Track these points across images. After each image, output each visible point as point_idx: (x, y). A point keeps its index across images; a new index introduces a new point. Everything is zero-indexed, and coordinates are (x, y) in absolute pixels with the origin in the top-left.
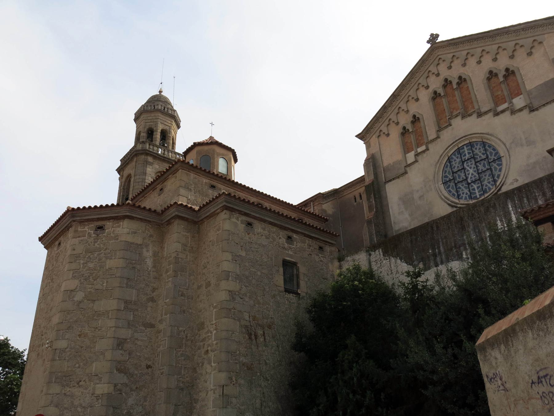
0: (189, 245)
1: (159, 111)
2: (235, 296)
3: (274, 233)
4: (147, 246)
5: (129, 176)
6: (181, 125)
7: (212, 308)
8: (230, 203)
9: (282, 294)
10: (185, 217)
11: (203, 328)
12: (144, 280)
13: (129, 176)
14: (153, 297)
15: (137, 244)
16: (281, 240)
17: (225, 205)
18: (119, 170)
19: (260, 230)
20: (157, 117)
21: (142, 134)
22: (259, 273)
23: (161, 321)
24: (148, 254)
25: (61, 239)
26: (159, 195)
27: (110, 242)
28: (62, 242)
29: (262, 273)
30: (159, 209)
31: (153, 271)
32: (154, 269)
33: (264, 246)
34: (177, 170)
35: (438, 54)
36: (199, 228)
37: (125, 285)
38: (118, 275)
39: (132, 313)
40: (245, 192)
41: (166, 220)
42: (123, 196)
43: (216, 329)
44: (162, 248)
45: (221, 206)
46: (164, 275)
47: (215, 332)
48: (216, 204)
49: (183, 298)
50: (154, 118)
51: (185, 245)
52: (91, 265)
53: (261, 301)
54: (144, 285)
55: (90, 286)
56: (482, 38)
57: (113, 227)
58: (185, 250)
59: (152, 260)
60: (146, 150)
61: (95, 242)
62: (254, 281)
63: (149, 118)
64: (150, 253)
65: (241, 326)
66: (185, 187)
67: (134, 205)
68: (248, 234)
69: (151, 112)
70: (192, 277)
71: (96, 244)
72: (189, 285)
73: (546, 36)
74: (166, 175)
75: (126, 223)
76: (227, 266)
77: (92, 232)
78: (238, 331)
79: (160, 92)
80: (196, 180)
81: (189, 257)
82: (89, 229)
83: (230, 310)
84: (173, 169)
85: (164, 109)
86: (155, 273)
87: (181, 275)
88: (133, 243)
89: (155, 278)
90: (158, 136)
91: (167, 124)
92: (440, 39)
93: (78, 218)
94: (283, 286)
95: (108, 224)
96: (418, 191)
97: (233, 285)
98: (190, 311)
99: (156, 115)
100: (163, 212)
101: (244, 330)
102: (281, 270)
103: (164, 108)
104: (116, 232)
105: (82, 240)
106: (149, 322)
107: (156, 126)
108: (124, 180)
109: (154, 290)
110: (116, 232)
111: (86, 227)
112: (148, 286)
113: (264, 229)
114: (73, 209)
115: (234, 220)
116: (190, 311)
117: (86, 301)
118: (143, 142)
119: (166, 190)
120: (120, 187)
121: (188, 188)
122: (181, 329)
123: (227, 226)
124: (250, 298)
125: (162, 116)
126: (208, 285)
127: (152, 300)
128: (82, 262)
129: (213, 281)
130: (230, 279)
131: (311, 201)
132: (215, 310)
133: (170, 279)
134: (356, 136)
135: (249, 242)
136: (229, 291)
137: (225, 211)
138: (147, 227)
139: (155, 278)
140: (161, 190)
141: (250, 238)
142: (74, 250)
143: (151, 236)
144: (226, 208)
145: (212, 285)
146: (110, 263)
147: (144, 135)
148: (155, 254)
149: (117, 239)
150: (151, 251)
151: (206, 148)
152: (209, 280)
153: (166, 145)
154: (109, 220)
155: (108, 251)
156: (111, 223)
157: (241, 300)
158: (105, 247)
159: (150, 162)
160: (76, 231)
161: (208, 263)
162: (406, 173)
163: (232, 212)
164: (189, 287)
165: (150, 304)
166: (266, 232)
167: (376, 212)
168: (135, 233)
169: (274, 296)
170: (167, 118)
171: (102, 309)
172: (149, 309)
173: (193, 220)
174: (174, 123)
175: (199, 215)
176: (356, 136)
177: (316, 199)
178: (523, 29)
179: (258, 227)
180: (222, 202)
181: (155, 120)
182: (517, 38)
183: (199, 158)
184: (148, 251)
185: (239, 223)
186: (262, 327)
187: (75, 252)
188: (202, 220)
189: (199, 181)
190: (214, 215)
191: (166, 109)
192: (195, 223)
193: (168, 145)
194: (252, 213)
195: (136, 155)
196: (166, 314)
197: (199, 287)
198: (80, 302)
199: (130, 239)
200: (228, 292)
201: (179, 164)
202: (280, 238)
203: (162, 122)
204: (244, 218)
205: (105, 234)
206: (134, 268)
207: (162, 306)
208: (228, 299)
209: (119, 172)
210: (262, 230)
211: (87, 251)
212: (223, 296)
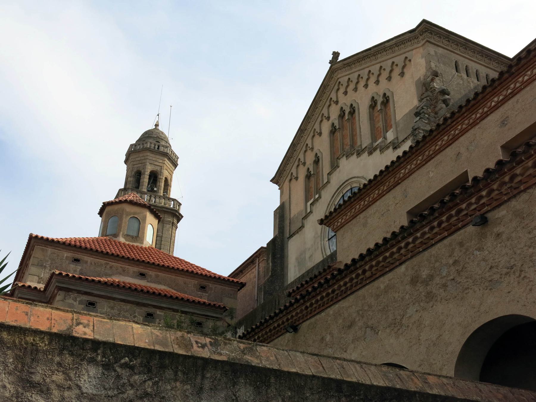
1: (149, 150)
3: (127, 311)
6: (178, 163)
20: (146, 157)
35: (339, 76)
40: (121, 262)
50: (143, 158)
56: (391, 47)
63: (137, 159)
66: (38, 265)
69: (139, 151)
73: (414, 51)
79: (157, 125)
80: (55, 255)
90: (145, 180)
91: (158, 164)
92: (340, 58)
96: (309, 249)
99: (145, 154)
107: (144, 168)
113: (112, 308)
115: (71, 301)
121: (42, 266)
131: (256, 257)
134: (271, 181)
144: (60, 289)
151: (116, 207)
153: (155, 189)
162: (303, 227)
167: (272, 276)
170: (157, 157)
174: (167, 162)
176: (271, 181)
177: (260, 254)
178: (397, 45)
181: (143, 161)
182: (394, 55)
189: (58, 256)
193: (158, 189)
194: (94, 292)
203: (152, 162)
204: (85, 298)
210: (109, 309)
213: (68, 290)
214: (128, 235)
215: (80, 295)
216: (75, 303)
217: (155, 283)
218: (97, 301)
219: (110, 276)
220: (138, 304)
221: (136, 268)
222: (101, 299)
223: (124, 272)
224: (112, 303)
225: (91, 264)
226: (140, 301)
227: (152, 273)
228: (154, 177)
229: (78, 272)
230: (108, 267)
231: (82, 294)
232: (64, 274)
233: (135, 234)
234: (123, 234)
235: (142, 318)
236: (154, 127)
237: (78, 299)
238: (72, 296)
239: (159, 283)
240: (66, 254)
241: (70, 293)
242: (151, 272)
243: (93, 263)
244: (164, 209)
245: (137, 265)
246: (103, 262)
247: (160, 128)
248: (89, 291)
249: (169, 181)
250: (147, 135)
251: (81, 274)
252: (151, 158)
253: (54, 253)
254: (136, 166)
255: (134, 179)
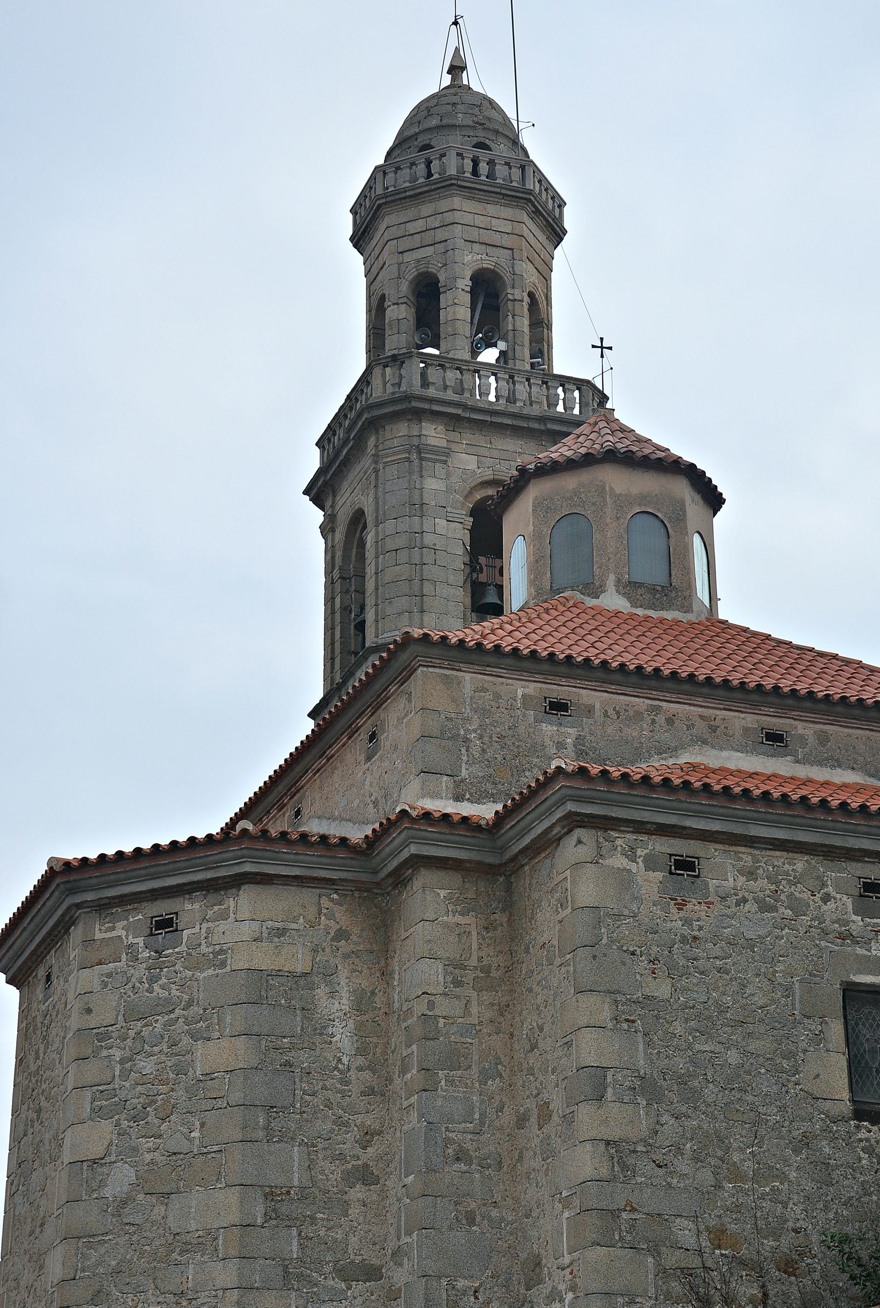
0: (474, 962)
2: (631, 1161)
4: (329, 975)
5: (358, 519)
7: (558, 1206)
8: (589, 801)
9: (842, 1128)
10: (447, 859)
11: (540, 1281)
12: (329, 1105)
13: (358, 519)
14: (366, 1165)
15: (292, 974)
16: (831, 905)
17: (570, 814)
18: (319, 491)
19: (732, 881)
20: (449, 217)
21: (392, 313)
22: (733, 1057)
23: (397, 1254)
24: (336, 1005)
25: (52, 959)
26: (369, 759)
27: (201, 976)
28: (55, 970)
29: (745, 1053)
30: (357, 834)
31: (360, 1069)
32: (360, 1061)
33: (750, 944)
34: (408, 672)
36: (509, 888)
37: (261, 1134)
38: (236, 1097)
39: (294, 1232)
40: (700, 701)
41: (385, 871)
42: (346, 609)
43: (573, 1288)
44: (385, 974)
45: (559, 814)
46: (397, 1081)
47: (570, 1296)
48: (543, 808)
49: (463, 1167)
50: (435, 222)
51: (455, 965)
52: (147, 1066)
53: (748, 1166)
54: (329, 1126)
55: (151, 1143)
57: (204, 919)
58: (458, 983)
59: (351, 1024)
60: (408, 398)
61: (153, 980)
62: (710, 1092)
63: (412, 227)
64: (344, 1002)
65: (663, 1272)
67: (265, 832)
68: (680, 906)
70: (493, 1085)
71: (156, 987)
72: (483, 1115)
74: (377, 686)
75: (245, 902)
76: (591, 1049)
77: (140, 941)
78: (652, 1291)
79: (457, 69)
80: (488, 696)
81: (474, 1010)
82: (126, 930)
83: (614, 1214)
84: (397, 665)
85: (475, 172)
86: (367, 1075)
87: (450, 1082)
88: (279, 973)
89: (370, 1092)
90: (457, 308)
91: (496, 239)
93: (90, 896)
94: (846, 1095)
95: (190, 909)
97: (621, 1119)
98: (495, 1213)
99: (443, 205)
100: (372, 842)
101: (676, 1286)
102: (836, 1030)
103: (475, 162)
104: (216, 939)
105: (109, 975)
106: (358, 1259)
108: (339, 535)
109: (368, 1137)
110: (216, 939)
111: (120, 925)
112: (346, 1124)
113: (751, 875)
114: (67, 864)
115: (619, 861)
116: (495, 1213)
117: (141, 1197)
118: (394, 358)
119: (386, 739)
120: (328, 572)
122: (461, 1284)
123: (587, 890)
124: (696, 1160)
125: (469, 205)
126: (545, 1114)
127: (365, 1176)
128: (118, 1054)
129: (557, 1104)
130: (610, 1094)
132: (566, 1214)
133: (414, 1099)
135: (684, 940)
136: (608, 1143)
137: (578, 833)
138: (325, 902)
139: (370, 1092)
140: (373, 737)
141: (687, 922)
142: (89, 1011)
143: (341, 934)
145: (555, 1117)
146: (210, 1056)
147: (400, 313)
148: (362, 1002)
149: (223, 964)
150: (345, 994)
152: (545, 1096)
154: (190, 892)
155: (196, 1010)
156: (196, 906)
157: (661, 1172)
158: (186, 997)
159: (435, 450)
160: (88, 942)
161: (541, 1029)
163: (606, 830)
164: (482, 1123)
165: (358, 1192)
166: (763, 883)
168: (281, 932)
169: (805, 1142)
170: (491, 209)
171: (193, 1226)
172: (354, 1211)
173: (479, 863)
175: (499, 843)
179: (723, 870)
180: (561, 802)
181: (440, 235)
183: (547, 531)
184: (333, 994)
185: (637, 868)
186: (757, 1269)
187: (93, 1021)
188: (514, 858)
189: (497, 696)
190: (547, 843)
191: (483, 168)
192: (488, 871)
195: (375, 425)
196: (409, 1233)
197: (522, 1121)
198: (124, 1203)
199: (264, 958)
200: (602, 1146)
201: (413, 649)
202: (826, 899)
203: (474, 234)
205: (183, 948)
206: (288, 1064)
207: (399, 1200)
208: (605, 1172)
209: (318, 501)
211: (132, 1014)
212: (586, 1163)
213: (605, 824)
214: (634, 585)
215: (645, 838)
216: (633, 867)
217: (820, 763)
218: (700, 853)
219: (673, 751)
220: (830, 853)
221: (750, 718)
222: (712, 847)
223: (714, 736)
224: (747, 856)
225: (606, 714)
226: (837, 842)
227: (803, 729)
228: (488, 289)
229: (570, 751)
230: (661, 719)
231: (649, 833)
232: (595, 769)
233: (660, 579)
234: (618, 581)
235: (849, 902)
236: (447, 80)
237: (639, 852)
238: (619, 842)
239: (837, 763)
240: (524, 689)
241: (614, 834)
242: (800, 725)
243: (611, 712)
244: (550, 426)
245: (755, 705)
246: (641, 703)
247: (473, 79)
248: (672, 820)
249: (542, 305)
250: (434, 122)
251: (580, 754)
252: (468, 219)
253: (484, 690)
254: (408, 257)
255: (409, 311)
